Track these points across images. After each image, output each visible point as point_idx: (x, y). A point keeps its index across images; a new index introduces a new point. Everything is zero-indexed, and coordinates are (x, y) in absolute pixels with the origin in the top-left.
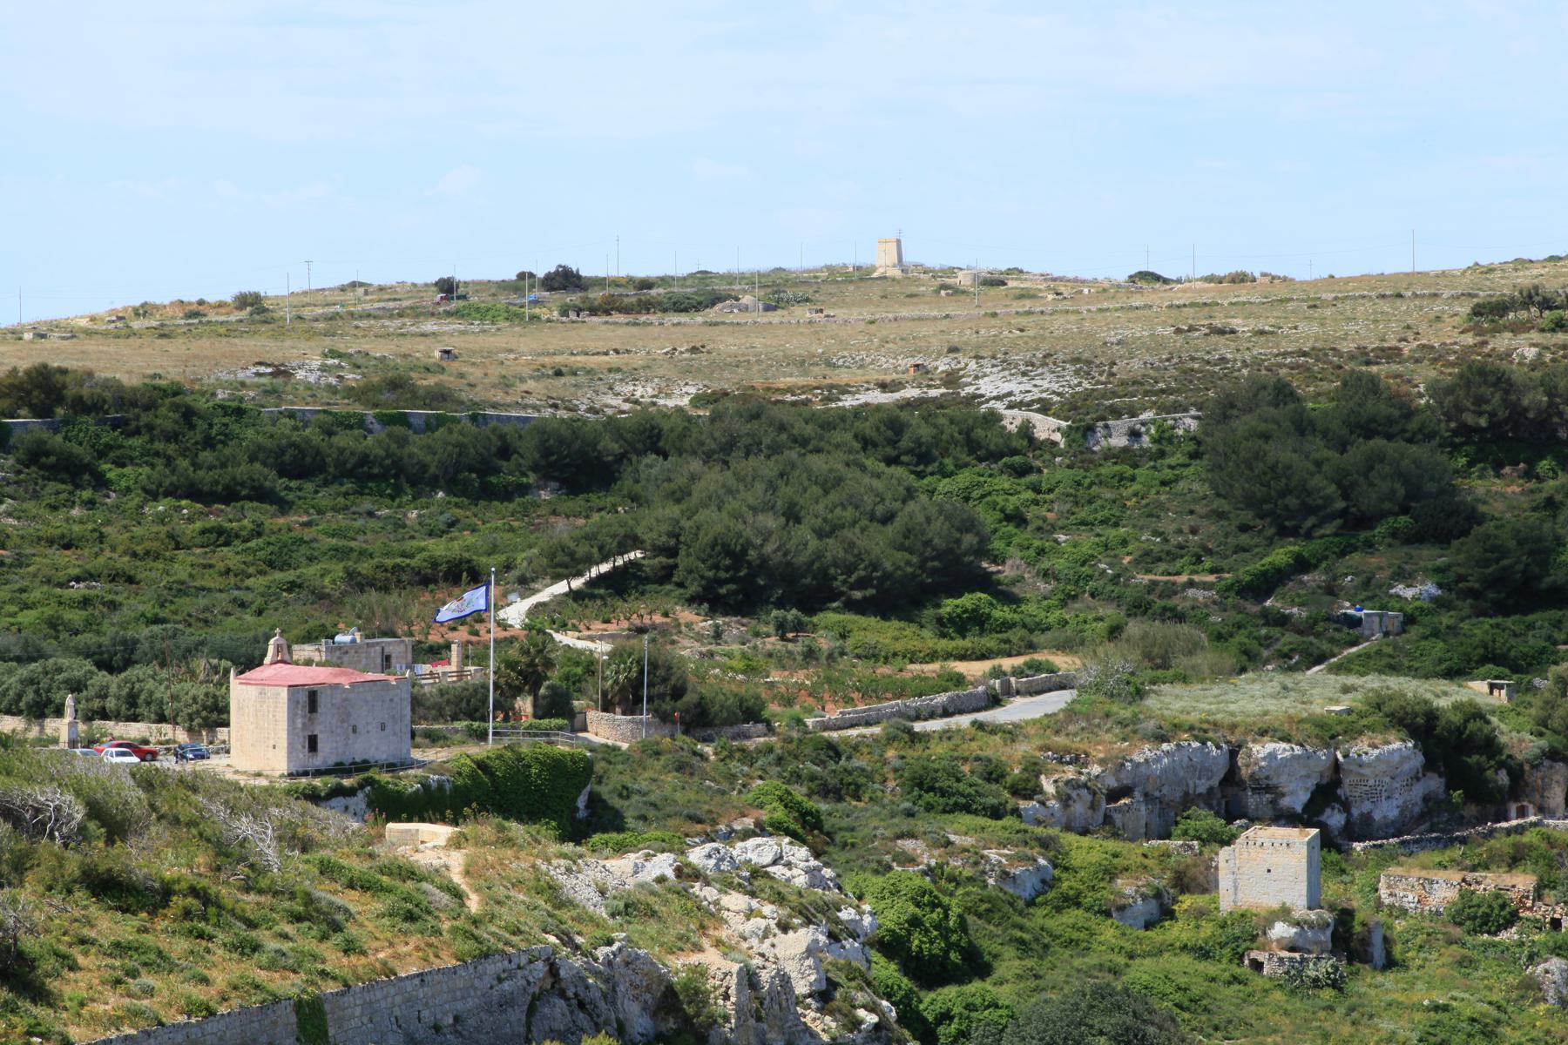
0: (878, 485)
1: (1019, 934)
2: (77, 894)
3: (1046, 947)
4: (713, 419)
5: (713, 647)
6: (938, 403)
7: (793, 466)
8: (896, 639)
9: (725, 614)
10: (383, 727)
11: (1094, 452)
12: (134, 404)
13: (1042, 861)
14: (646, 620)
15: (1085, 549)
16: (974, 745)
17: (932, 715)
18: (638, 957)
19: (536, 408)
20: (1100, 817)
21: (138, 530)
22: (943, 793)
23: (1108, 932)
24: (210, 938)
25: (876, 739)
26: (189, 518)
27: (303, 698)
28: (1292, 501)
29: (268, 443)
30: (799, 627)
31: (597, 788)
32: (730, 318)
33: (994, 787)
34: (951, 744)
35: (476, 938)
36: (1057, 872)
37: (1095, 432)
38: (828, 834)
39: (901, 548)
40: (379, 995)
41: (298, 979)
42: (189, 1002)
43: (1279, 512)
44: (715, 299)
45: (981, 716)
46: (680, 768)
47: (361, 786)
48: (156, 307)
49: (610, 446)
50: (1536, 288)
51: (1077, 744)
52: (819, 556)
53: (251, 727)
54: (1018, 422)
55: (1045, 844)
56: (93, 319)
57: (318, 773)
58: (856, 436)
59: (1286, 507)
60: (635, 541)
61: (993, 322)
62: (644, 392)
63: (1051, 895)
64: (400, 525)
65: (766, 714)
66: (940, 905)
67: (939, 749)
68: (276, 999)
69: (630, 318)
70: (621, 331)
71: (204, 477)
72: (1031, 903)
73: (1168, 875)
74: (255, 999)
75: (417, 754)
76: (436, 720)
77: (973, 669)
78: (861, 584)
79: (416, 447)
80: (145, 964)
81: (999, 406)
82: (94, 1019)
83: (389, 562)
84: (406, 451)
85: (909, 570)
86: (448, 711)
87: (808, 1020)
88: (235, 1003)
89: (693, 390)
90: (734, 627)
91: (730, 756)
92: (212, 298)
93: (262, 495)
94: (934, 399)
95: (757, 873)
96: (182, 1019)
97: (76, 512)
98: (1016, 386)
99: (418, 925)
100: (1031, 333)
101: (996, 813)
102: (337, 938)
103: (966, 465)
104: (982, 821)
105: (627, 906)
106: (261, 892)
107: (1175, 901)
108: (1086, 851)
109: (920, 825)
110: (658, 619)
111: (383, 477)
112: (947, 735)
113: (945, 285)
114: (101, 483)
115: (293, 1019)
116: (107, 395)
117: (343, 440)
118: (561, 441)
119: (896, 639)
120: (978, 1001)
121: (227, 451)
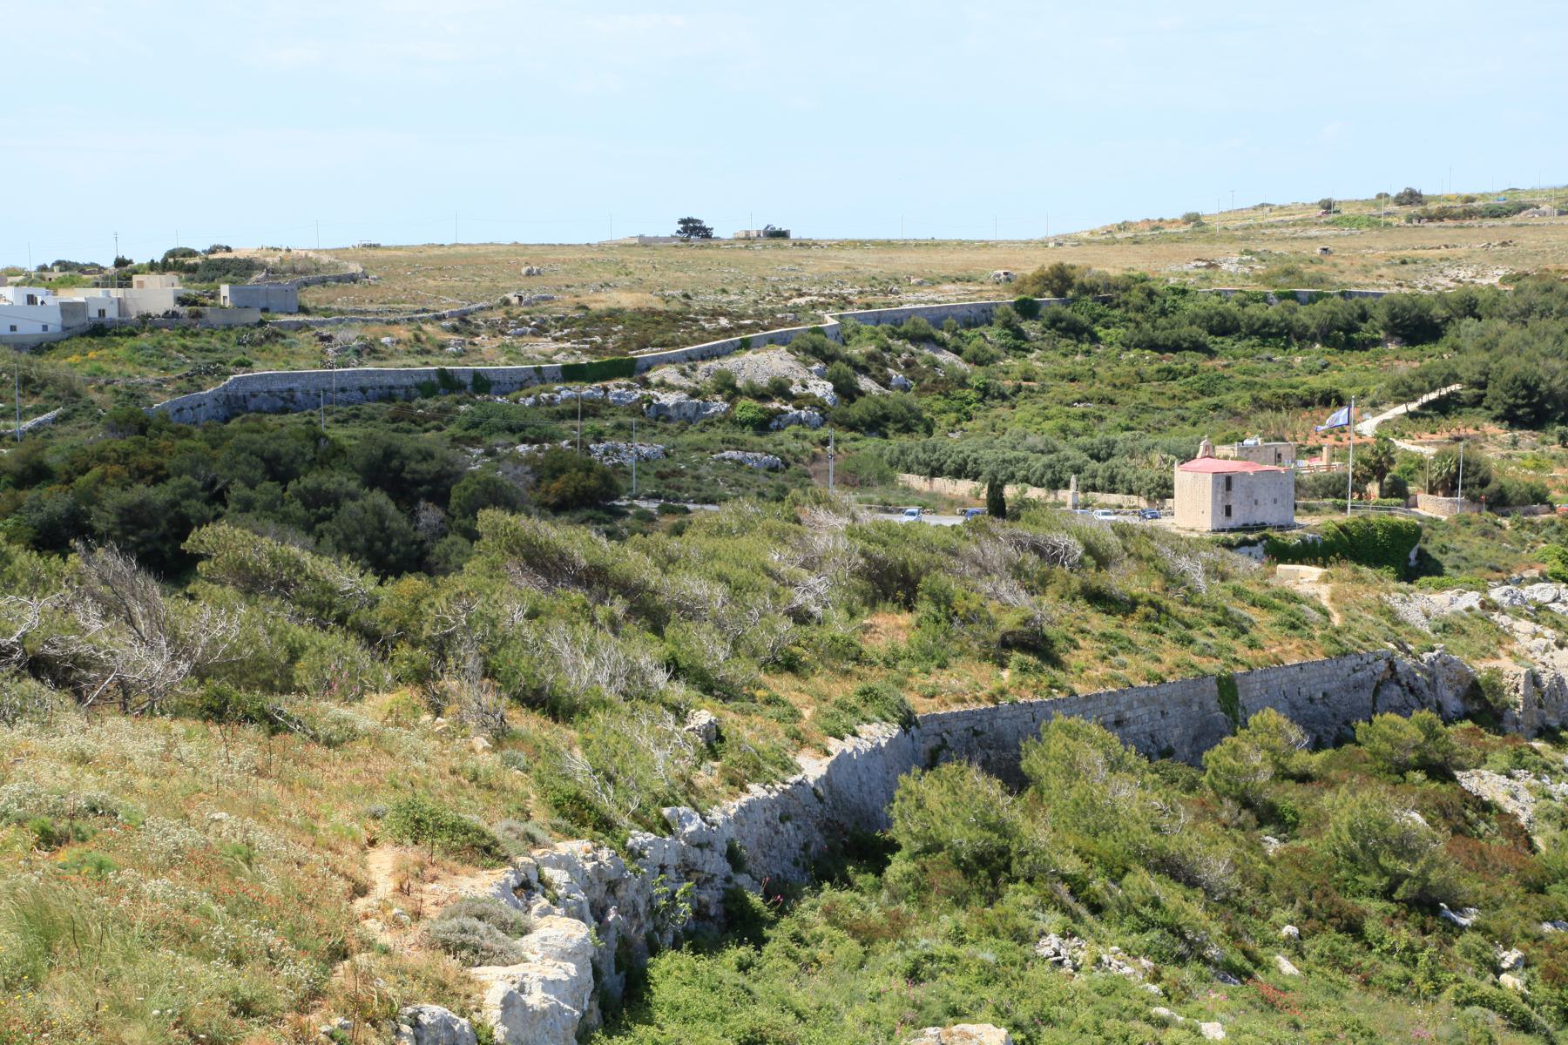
2: (1079, 602)
5: (1511, 452)
9: (1521, 428)
10: (1275, 501)
12: (1116, 288)
14: (1462, 433)
19: (1386, 286)
24: (1162, 634)
26: (1149, 361)
27: (1223, 481)
31: (1424, 546)
35: (1338, 643)
40: (1272, 676)
44: (1521, 208)
46: (1485, 534)
47: (1260, 540)
48: (1132, 224)
49: (1439, 312)
57: (1232, 530)
60: (1455, 378)
62: (1465, 274)
64: (1289, 367)
65: (1549, 498)
68: (1205, 676)
70: (1449, 232)
71: (1160, 336)
74: (1191, 675)
75: (1298, 520)
76: (1311, 497)
79: (1304, 315)
80: (1121, 648)
82: (1089, 680)
83: (1281, 392)
84: (1295, 317)
86: (1320, 492)
88: (1178, 676)
89: (1502, 273)
90: (1527, 437)
91: (1522, 527)
92: (1168, 218)
93: (1198, 347)
95: (1540, 607)
96: (1144, 684)
97: (1079, 358)
102: (1245, 638)
106: (1194, 606)
110: (1471, 431)
111: (1279, 335)
114: (1095, 339)
115: (1216, 688)
116: (1099, 281)
117: (1253, 310)
118: (1404, 309)
121: (1175, 318)
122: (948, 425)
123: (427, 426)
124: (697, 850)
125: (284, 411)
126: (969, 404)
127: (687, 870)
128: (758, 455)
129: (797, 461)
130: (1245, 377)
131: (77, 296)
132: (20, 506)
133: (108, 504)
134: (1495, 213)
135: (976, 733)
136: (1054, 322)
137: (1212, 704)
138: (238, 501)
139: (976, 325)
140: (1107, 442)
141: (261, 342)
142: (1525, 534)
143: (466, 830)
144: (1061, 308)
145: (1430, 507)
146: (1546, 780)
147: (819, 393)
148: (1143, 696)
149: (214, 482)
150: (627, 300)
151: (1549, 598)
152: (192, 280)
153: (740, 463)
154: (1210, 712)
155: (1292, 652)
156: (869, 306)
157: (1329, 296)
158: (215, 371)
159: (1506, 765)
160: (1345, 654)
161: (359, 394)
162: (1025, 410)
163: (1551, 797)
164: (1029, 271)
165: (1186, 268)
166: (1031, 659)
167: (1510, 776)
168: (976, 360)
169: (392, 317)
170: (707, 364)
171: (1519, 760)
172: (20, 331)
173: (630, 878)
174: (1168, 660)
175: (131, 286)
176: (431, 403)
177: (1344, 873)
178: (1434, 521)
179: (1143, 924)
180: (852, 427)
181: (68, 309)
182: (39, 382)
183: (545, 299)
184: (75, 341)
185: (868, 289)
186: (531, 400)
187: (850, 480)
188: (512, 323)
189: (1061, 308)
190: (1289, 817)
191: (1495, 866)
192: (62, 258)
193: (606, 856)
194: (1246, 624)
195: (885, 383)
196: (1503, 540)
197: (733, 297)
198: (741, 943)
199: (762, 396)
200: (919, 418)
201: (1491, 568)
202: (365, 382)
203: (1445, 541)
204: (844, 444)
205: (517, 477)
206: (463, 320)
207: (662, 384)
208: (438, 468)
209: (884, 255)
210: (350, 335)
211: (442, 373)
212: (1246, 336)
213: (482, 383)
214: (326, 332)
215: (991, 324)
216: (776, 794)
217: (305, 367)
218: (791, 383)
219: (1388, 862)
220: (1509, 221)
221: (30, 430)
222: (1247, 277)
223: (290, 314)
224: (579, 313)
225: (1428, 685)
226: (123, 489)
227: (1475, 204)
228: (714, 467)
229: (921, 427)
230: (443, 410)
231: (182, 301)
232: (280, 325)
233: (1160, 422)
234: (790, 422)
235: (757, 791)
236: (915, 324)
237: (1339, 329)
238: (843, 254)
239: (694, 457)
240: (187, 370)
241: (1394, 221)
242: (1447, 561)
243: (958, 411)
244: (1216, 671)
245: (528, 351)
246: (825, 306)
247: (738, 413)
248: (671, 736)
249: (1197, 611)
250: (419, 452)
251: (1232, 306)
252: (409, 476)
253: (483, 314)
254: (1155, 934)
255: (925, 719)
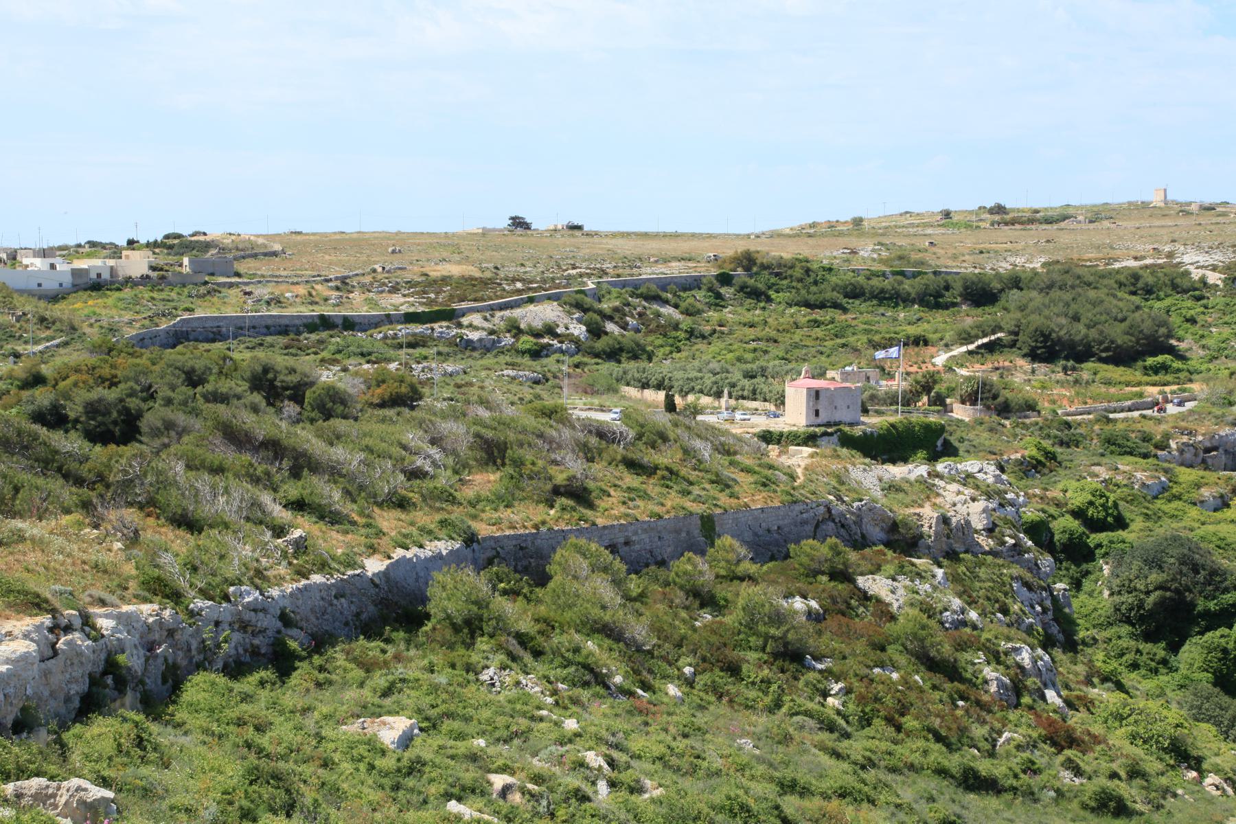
0: (1121, 304)
1: (1146, 511)
2: (620, 467)
3: (1159, 517)
4: (1048, 273)
5: (1031, 377)
6: (1161, 266)
7: (1080, 295)
8: (1121, 375)
9: (1040, 362)
10: (848, 407)
12: (785, 266)
13: (1163, 479)
14: (1001, 364)
15: (1224, 336)
16: (1139, 425)
17: (1122, 411)
18: (875, 507)
19: (966, 268)
20: (1199, 460)
21: (781, 320)
22: (1119, 446)
23: (1194, 512)
24: (671, 488)
25: (1090, 421)
26: (803, 315)
27: (813, 393)
29: (839, 282)
30: (1074, 369)
31: (949, 438)
32: (1072, 227)
33: (1146, 444)
34: (1127, 424)
35: (792, 495)
36: (1171, 484)
38: (1059, 463)
39: (1128, 333)
40: (741, 515)
41: (704, 507)
42: (652, 512)
44: (1065, 218)
45: (1144, 412)
46: (991, 430)
47: (836, 432)
48: (818, 223)
49: (996, 285)
51: (1191, 426)
52: (1086, 336)
54: (1200, 275)
55: (1166, 471)
56: (791, 229)
57: (819, 426)
58: (1116, 282)
60: (1000, 329)
61: (1199, 228)
62: (1019, 261)
63: (1166, 494)
64: (895, 320)
65: (1037, 408)
66: (1105, 496)
67: (1120, 426)
68: (691, 514)
69: (1022, 227)
70: (1016, 233)
71: (812, 298)
72: (1156, 497)
73: (1230, 487)
74: (681, 514)
75: (862, 419)
76: (883, 405)
77: (1153, 390)
78: (1106, 350)
79: (907, 286)
80: (639, 497)
81: (1191, 268)
82: (610, 517)
83: (888, 336)
84: (901, 287)
85: (1130, 344)
86: (889, 401)
87: (980, 541)
88: (672, 514)
89: (1043, 260)
90: (1042, 368)
91: (1017, 426)
92: (842, 220)
93: (836, 306)
94: (1159, 264)
95: (969, 476)
96: (647, 519)
97: (757, 312)
98: (1202, 259)
99: (767, 488)
100: (1215, 233)
101: (1145, 456)
102: (728, 491)
103: (1170, 295)
104: (1137, 459)
105: (890, 487)
106: (700, 471)
107: (1231, 499)
108: (1187, 475)
109: (1104, 460)
110: (1007, 364)
111: (890, 299)
112: (1126, 420)
113: (1184, 210)
114: (769, 300)
115: (699, 522)
116: (774, 262)
117: (875, 282)
118: (973, 283)
119: (1121, 375)
120: (1115, 539)
121: (823, 286)
122: (664, 354)
123: (309, 351)
124: (253, 613)
125: (213, 341)
126: (680, 341)
127: (244, 626)
128: (527, 373)
129: (555, 377)
130: (866, 326)
131: (82, 264)
132: (20, 401)
133: (77, 400)
134: (1048, 221)
135: (522, 548)
136: (742, 288)
137: (696, 532)
138: (163, 399)
139: (690, 289)
140: (762, 367)
141: (204, 296)
142: (1018, 430)
143: (26, 593)
144: (747, 279)
145: (961, 412)
146: (917, 582)
147: (576, 333)
148: (645, 526)
149: (150, 386)
150: (455, 270)
151: (976, 470)
152: (169, 254)
153: (514, 378)
154: (694, 537)
155: (757, 500)
156: (619, 276)
157: (926, 273)
158: (169, 314)
159: (892, 572)
160: (795, 502)
161: (265, 330)
162: (717, 345)
163: (917, 593)
164: (730, 253)
165: (835, 254)
166: (571, 503)
167: (894, 580)
168: (688, 313)
169: (295, 280)
170: (502, 313)
171: (901, 570)
172: (44, 286)
173: (185, 628)
174: (669, 504)
175: (121, 258)
176: (314, 337)
177: (742, 636)
178: (960, 422)
179: (565, 663)
180: (597, 355)
181: (75, 273)
182: (50, 320)
183: (400, 269)
184: (80, 293)
185: (620, 265)
186: (381, 335)
187: (589, 390)
188: (376, 284)
189: (747, 279)
190: (722, 602)
191: (856, 632)
192: (91, 239)
193: (168, 614)
194: (731, 483)
195: (624, 327)
196: (1003, 434)
197: (528, 269)
198: (267, 669)
199: (538, 335)
200: (644, 350)
201: (990, 452)
202: (269, 322)
203: (964, 435)
204: (589, 367)
205: (354, 386)
206: (344, 283)
207: (470, 326)
208: (299, 379)
209: (640, 243)
210: (263, 292)
211: (322, 317)
212: (869, 299)
213: (349, 324)
214: (248, 289)
215: (700, 289)
216: (333, 581)
217: (230, 312)
218: (558, 326)
219: (761, 628)
220: (1055, 226)
221: (40, 352)
222: (874, 260)
223: (228, 277)
224: (424, 278)
225: (854, 522)
226: (88, 391)
227: (1038, 215)
228: (496, 381)
229: (645, 356)
230: (321, 342)
231: (153, 268)
232: (219, 284)
233: (806, 355)
234: (555, 352)
235: (317, 578)
236: (648, 288)
237: (931, 296)
238: (614, 241)
239: (483, 374)
240: (150, 314)
241: (982, 224)
242: (962, 448)
243: (672, 346)
244: (700, 511)
245: (383, 303)
246: (589, 276)
247: (520, 346)
248: (266, 544)
249: (700, 474)
250: (287, 368)
251: (861, 279)
252: (279, 384)
253: (358, 278)
254: (572, 669)
255: (484, 539)
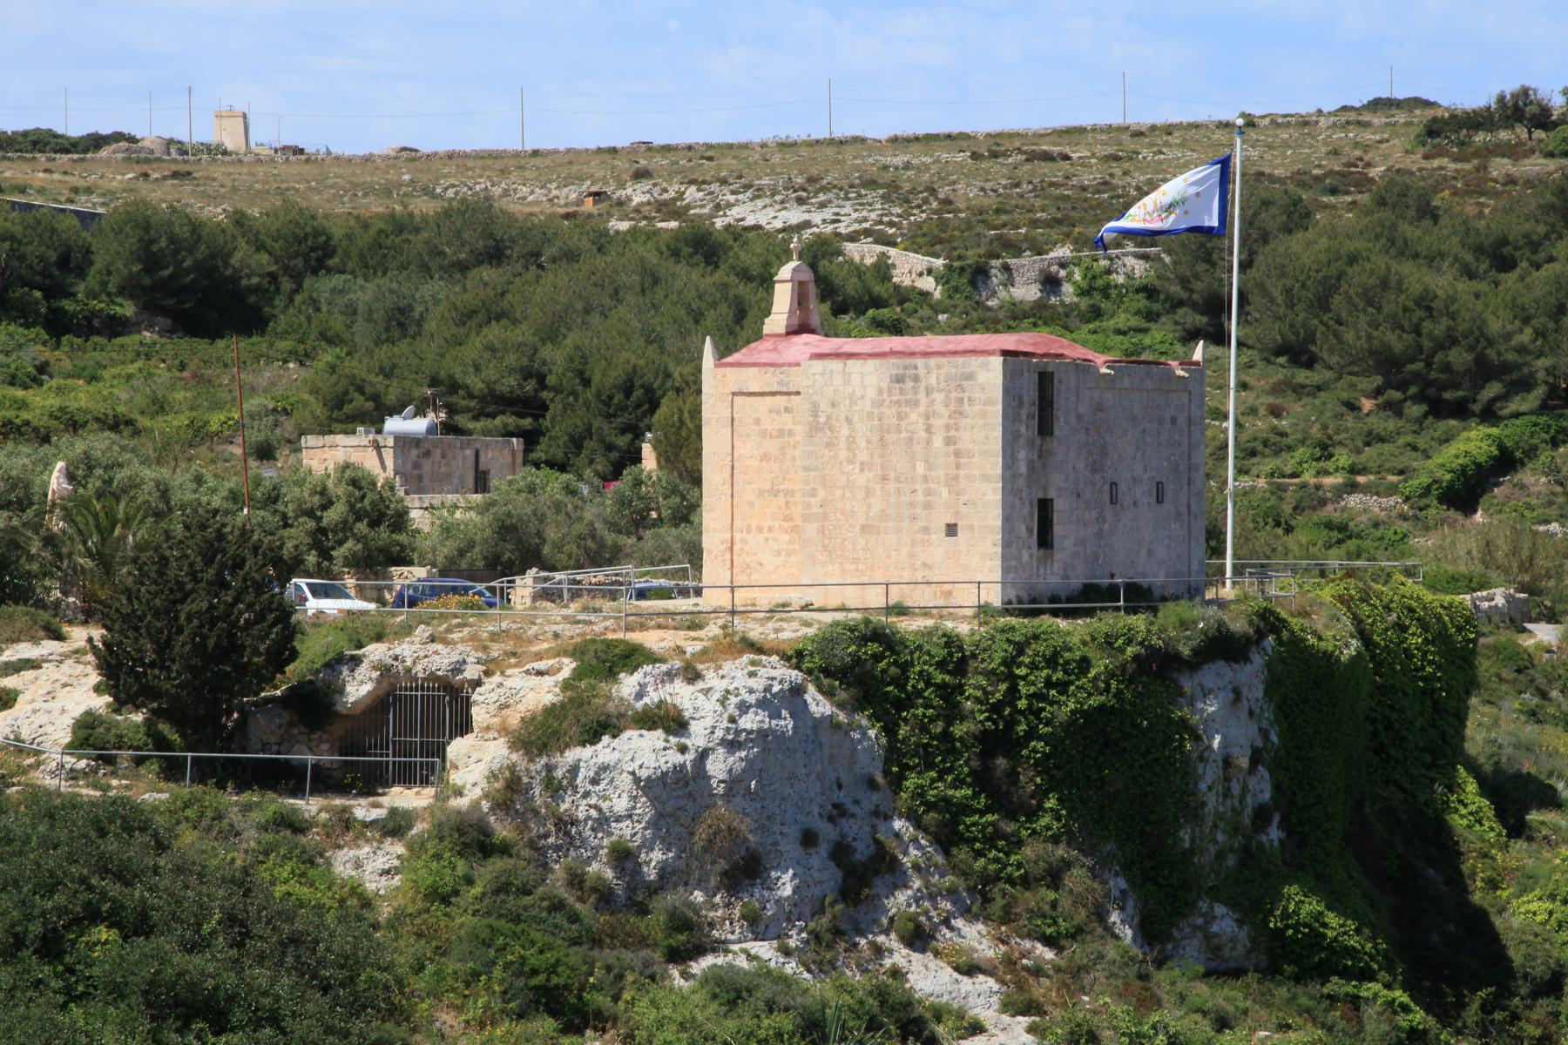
11: (989, 309)
28: (1459, 357)
37: (989, 277)
43: (1433, 375)
49: (250, 263)
50: (1525, 92)
53: (861, 479)
59: (1447, 368)
